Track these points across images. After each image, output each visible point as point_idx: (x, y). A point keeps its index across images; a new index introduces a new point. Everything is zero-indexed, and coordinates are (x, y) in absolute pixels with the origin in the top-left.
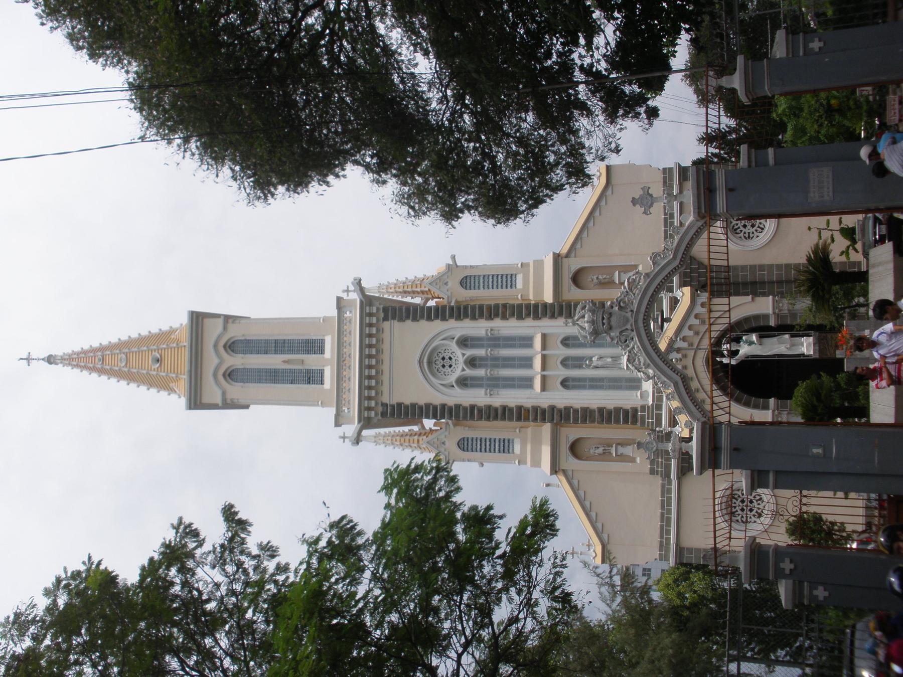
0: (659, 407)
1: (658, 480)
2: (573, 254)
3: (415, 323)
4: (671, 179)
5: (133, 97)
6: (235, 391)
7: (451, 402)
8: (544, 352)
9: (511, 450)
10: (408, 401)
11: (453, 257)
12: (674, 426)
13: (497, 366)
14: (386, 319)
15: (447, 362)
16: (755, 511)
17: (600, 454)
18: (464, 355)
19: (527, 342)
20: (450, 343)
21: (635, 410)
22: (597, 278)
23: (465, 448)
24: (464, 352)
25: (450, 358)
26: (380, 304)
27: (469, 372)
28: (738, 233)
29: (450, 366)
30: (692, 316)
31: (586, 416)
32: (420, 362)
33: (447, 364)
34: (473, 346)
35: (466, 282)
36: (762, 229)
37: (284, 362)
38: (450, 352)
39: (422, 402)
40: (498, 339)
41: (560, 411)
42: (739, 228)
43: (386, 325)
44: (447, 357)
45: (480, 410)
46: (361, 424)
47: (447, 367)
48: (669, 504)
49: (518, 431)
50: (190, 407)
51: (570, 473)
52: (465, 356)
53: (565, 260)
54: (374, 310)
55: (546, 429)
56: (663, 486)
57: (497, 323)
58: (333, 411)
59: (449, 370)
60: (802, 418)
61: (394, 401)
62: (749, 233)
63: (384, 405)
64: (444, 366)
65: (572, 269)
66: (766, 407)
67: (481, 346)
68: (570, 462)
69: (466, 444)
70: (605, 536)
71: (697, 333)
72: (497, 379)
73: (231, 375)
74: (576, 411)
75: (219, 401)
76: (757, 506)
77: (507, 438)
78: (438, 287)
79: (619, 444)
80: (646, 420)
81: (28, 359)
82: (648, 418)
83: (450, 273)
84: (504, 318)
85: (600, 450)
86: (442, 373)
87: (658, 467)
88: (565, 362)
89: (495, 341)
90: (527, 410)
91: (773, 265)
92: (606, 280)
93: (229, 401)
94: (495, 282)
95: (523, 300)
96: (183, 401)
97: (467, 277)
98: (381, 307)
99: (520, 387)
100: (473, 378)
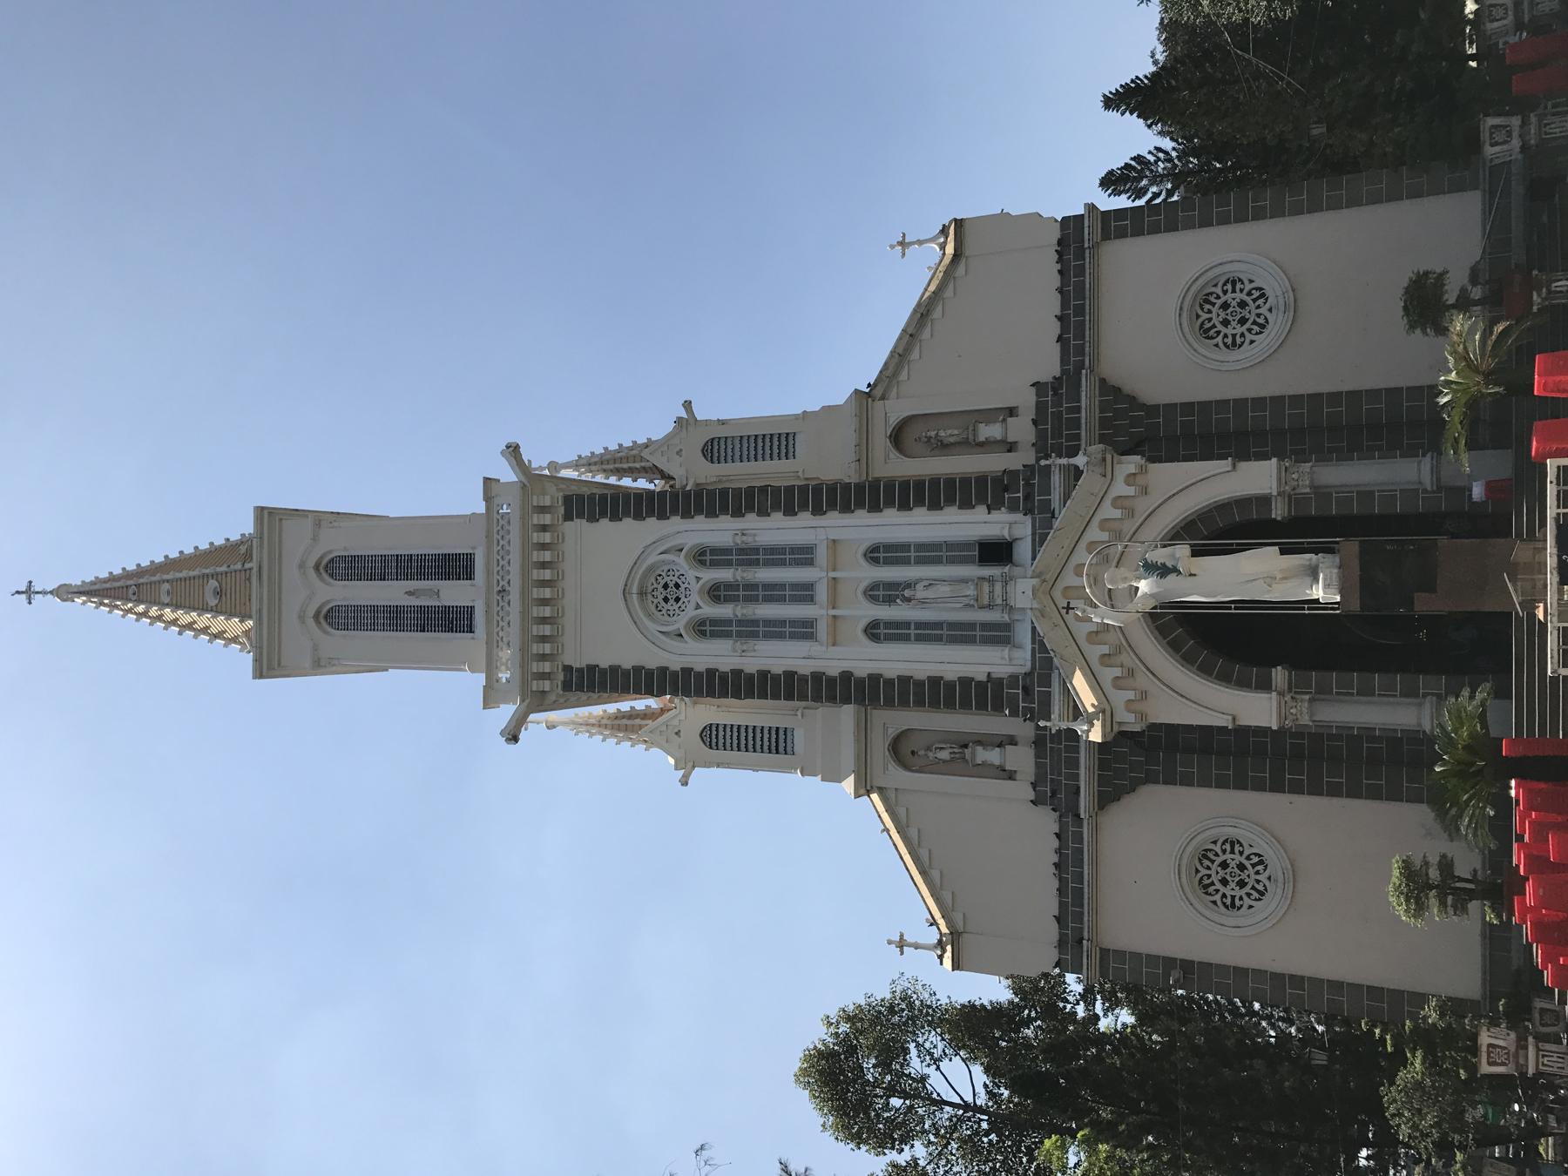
1: (1046, 822)
2: (894, 393)
7: (675, 664)
9: (789, 749)
10: (604, 663)
11: (688, 405)
13: (752, 599)
14: (568, 517)
15: (672, 592)
19: (802, 555)
20: (676, 559)
23: (714, 744)
25: (677, 586)
28: (1212, 338)
30: (1107, 502)
31: (906, 692)
32: (625, 593)
34: (715, 564)
35: (714, 449)
36: (1261, 894)
37: (410, 593)
38: (677, 574)
39: (627, 664)
40: (756, 550)
46: (526, 703)
47: (672, 601)
49: (799, 713)
50: (260, 672)
55: (847, 714)
57: (751, 521)
58: (481, 679)
59: (676, 607)
63: (568, 669)
64: (666, 600)
66: (1265, 685)
67: (728, 564)
68: (897, 776)
72: (755, 623)
76: (1253, 877)
77: (782, 725)
79: (979, 743)
81: (29, 592)
84: (763, 512)
86: (664, 612)
89: (749, 555)
91: (1247, 399)
92: (952, 440)
94: (783, 447)
95: (807, 479)
96: (245, 661)
97: (713, 439)
100: (714, 622)
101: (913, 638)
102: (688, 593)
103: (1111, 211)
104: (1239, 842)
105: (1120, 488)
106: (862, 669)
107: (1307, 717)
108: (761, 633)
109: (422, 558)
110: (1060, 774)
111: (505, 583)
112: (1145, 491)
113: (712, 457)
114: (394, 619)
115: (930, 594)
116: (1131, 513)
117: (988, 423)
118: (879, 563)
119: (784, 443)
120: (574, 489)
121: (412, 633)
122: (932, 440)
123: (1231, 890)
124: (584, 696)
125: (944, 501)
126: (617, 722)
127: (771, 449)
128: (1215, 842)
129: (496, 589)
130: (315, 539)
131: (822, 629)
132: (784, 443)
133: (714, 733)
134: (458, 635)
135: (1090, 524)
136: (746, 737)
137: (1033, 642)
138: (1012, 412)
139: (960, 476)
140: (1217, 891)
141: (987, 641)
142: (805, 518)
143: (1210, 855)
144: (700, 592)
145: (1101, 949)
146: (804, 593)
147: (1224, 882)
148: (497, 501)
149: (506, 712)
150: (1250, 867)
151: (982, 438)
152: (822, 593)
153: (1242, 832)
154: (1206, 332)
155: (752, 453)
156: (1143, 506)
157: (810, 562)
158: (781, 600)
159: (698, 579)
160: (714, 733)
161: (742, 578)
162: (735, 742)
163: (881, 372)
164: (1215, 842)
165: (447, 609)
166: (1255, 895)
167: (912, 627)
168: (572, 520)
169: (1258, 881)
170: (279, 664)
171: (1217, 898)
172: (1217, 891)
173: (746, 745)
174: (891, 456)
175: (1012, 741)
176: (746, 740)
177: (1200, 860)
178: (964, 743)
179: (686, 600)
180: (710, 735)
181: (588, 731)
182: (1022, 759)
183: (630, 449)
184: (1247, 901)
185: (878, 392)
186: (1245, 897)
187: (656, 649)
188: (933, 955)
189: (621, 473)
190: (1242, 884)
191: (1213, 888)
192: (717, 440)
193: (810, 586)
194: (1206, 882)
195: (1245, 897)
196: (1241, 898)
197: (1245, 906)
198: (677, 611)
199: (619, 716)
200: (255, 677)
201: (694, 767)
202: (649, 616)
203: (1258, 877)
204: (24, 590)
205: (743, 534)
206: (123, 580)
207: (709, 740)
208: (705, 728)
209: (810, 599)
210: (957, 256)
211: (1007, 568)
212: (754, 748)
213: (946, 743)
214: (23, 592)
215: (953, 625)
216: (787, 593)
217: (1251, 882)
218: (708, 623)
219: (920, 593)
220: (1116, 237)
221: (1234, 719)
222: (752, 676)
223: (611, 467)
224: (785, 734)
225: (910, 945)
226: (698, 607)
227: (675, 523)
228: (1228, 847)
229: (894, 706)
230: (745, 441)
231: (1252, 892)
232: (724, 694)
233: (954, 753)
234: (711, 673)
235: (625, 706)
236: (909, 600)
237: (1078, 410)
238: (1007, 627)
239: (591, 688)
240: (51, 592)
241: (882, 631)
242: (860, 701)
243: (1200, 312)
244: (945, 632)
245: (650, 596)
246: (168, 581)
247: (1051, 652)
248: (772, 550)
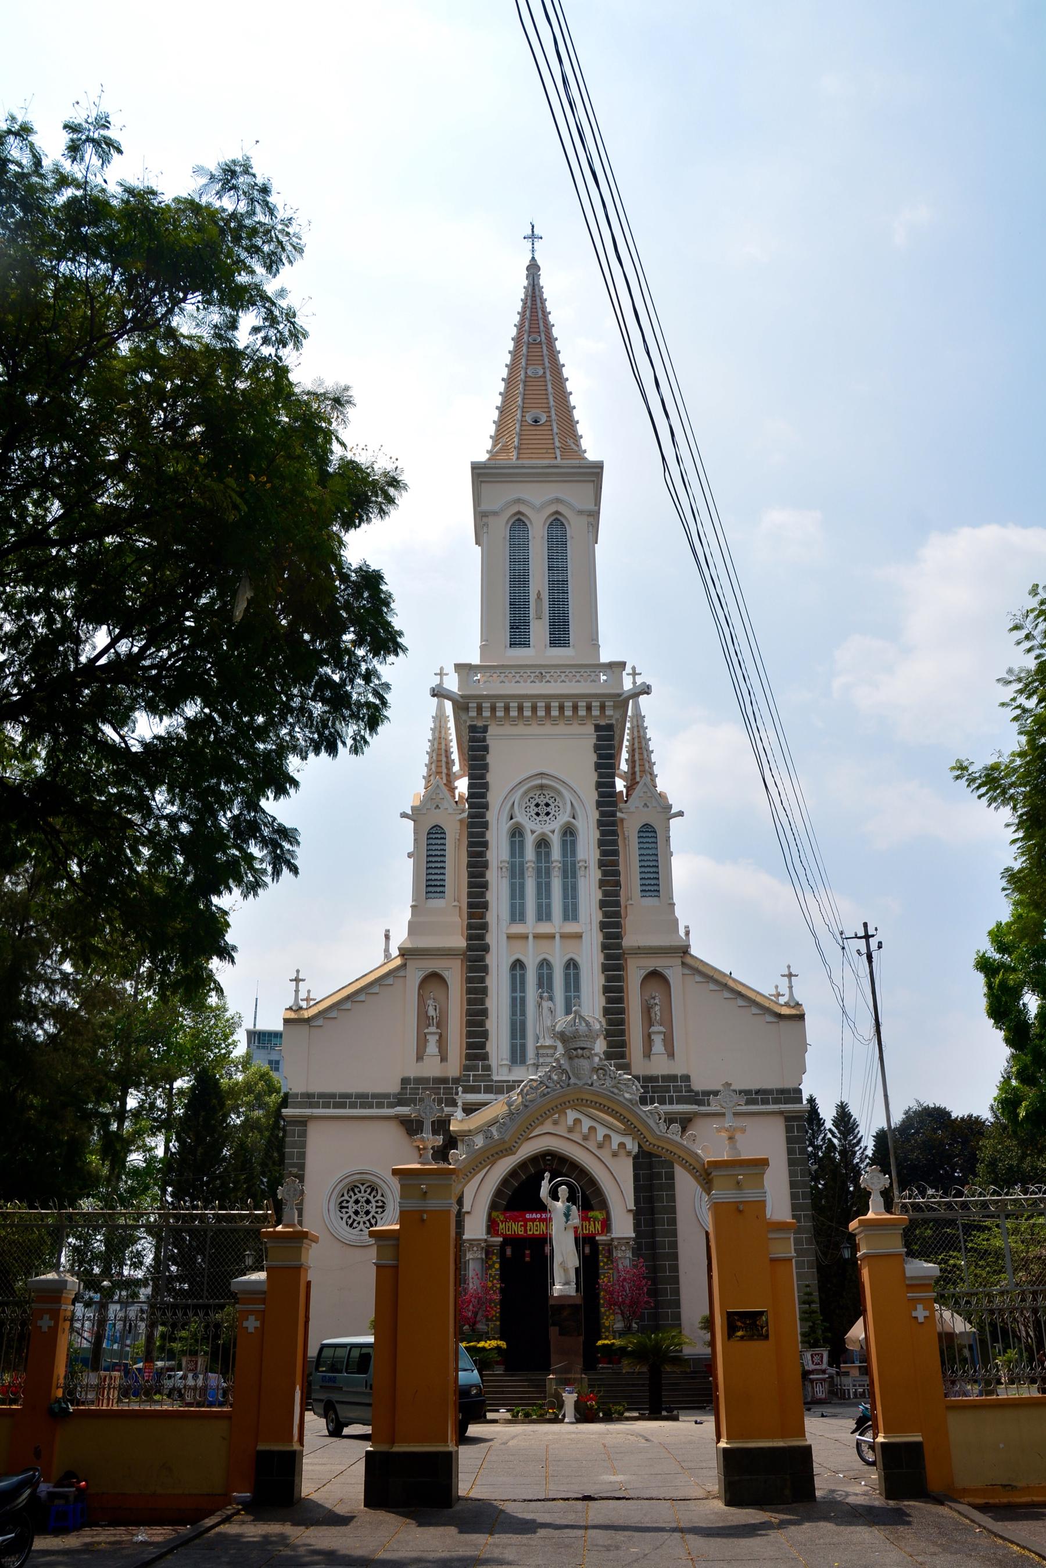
0: (488, 1090)
1: (393, 1087)
2: (687, 972)
3: (592, 767)
6: (500, 528)
7: (491, 816)
8: (557, 936)
10: (491, 759)
12: (464, 1110)
14: (598, 728)
15: (543, 810)
16: (355, 1218)
17: (427, 1012)
18: (553, 832)
19: (571, 913)
21: (485, 1057)
22: (656, 1004)
23: (431, 836)
26: (617, 720)
27: (530, 841)
29: (538, 814)
32: (542, 775)
33: (542, 810)
34: (564, 843)
36: (351, 1226)
38: (556, 814)
40: (574, 875)
41: (482, 959)
42: (355, 1194)
43: (590, 729)
44: (549, 809)
45: (482, 854)
46: (460, 700)
47: (536, 810)
48: (363, 1106)
49: (456, 903)
51: (402, 974)
52: (550, 834)
53: (679, 961)
54: (608, 712)
55: (460, 942)
56: (386, 1096)
58: (475, 659)
59: (533, 813)
61: (491, 742)
62: (347, 1207)
63: (485, 729)
64: (537, 805)
65: (667, 971)
68: (415, 975)
69: (437, 836)
70: (320, 1022)
71: (585, 1138)
73: (519, 523)
74: (482, 980)
75: (484, 507)
77: (446, 889)
78: (641, 795)
79: (441, 1036)
80: (471, 1073)
81: (533, 237)
82: (474, 1075)
83: (660, 810)
84: (602, 883)
85: (431, 1012)
86: (528, 804)
87: (411, 1089)
88: (545, 965)
89: (570, 872)
90: (482, 916)
92: (653, 1015)
93: (485, 520)
95: (626, 907)
97: (655, 832)
98: (614, 722)
100: (522, 844)
102: (543, 823)
104: (384, 1211)
105: (616, 1139)
106: (491, 959)
107: (471, 1257)
109: (565, 602)
110: (653, 1092)
111: (548, 678)
112: (615, 1155)
114: (519, 580)
115: (545, 1011)
116: (600, 1146)
117: (664, 1040)
119: (652, 888)
120: (617, 732)
121: (508, 594)
122: (652, 1001)
123: (352, 1207)
124: (466, 745)
125: (609, 997)
126: (443, 752)
127: (648, 878)
128: (382, 1196)
129: (543, 671)
130: (581, 512)
131: (518, 929)
132: (652, 888)
134: (508, 634)
135: (621, 1522)
136: (437, 874)
137: (514, 1081)
138: (671, 1055)
139: (622, 922)
140: (351, 1197)
141: (513, 1048)
142: (597, 916)
143: (374, 1193)
144: (543, 834)
145: (306, 1121)
146: (544, 914)
147: (357, 1202)
148: (609, 671)
149: (452, 683)
150: (368, 1218)
151: (653, 1037)
152: (544, 928)
153: (391, 1213)
154: (352, 1189)
156: (605, 1154)
157: (566, 918)
159: (553, 832)
161: (554, 867)
162: (434, 853)
163: (702, 961)
164: (382, 1196)
165: (527, 624)
166: (350, 1222)
167: (522, 994)
168: (595, 731)
169: (359, 1223)
170: (481, 482)
171: (346, 1197)
172: (351, 1197)
173: (431, 868)
174: (642, 971)
175: (444, 1059)
176: (435, 862)
177: (370, 1186)
178: (441, 1023)
179: (537, 821)
181: (435, 727)
182: (432, 1068)
183: (649, 761)
184: (345, 1216)
185: (688, 960)
186: (348, 1215)
187: (501, 799)
188: (290, 1002)
189: (632, 752)
190: (356, 1213)
191: (353, 1195)
193: (549, 918)
194: (356, 1190)
195: (348, 1215)
196: (347, 1212)
197: (342, 1215)
198: (529, 814)
199: (448, 753)
200: (472, 463)
201: (414, 821)
202: (526, 793)
203: (362, 1223)
204: (536, 232)
205: (586, 867)
206: (544, 329)
209: (539, 919)
210: (780, 1016)
212: (429, 874)
213: (440, 1013)
214: (533, 232)
215: (523, 1024)
216: (544, 901)
217: (358, 1219)
218: (521, 839)
219: (546, 1004)
221: (468, 1213)
223: (636, 745)
224: (440, 892)
225: (297, 986)
226: (533, 832)
227: (594, 815)
228: (380, 1204)
230: (654, 858)
231: (352, 1220)
233: (433, 1019)
234: (485, 844)
235: (455, 756)
236: (541, 998)
237: (671, 1103)
238: (523, 1061)
239: (471, 748)
240: (533, 258)
241: (518, 972)
243: (365, 1186)
245: (538, 793)
246: (544, 373)
248: (574, 888)
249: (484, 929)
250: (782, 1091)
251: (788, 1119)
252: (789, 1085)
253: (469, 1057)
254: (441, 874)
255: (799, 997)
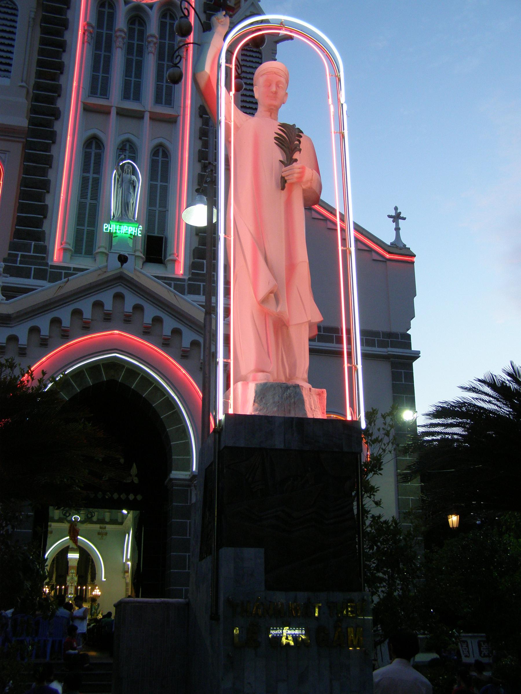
0: (41, 275)
4: (394, 345)
5: (35, 389)
13: (129, 50)
24: (155, 8)
30: (159, 313)
49: (24, 84)
52: (148, 9)
60: (374, 439)
72: (109, 48)
77: (13, 69)
80: (20, 253)
82: (22, 256)
99: (94, 80)
100: (112, 17)
101: (85, 175)
103: (413, 371)
108: (99, 52)
113: (247, 50)
118: (154, 155)
133: (10, 11)
137: (75, 269)
155: (248, 59)
158: (128, 72)
160: (10, 11)
167: (95, 176)
180: (8, 8)
192: (260, 56)
207: (3, 5)
208: (15, 4)
211: (142, 255)
220: (393, 373)
222: (62, 36)
224: (5, 71)
229: (16, 225)
232: (23, 195)
241: (93, 151)
242: (32, 133)
244: (89, 201)
247: (66, 279)
249: (55, 92)
250: (390, 335)
251: (394, 365)
252: (395, 329)
253: (17, 234)
254: (8, 52)
255: (407, 240)
